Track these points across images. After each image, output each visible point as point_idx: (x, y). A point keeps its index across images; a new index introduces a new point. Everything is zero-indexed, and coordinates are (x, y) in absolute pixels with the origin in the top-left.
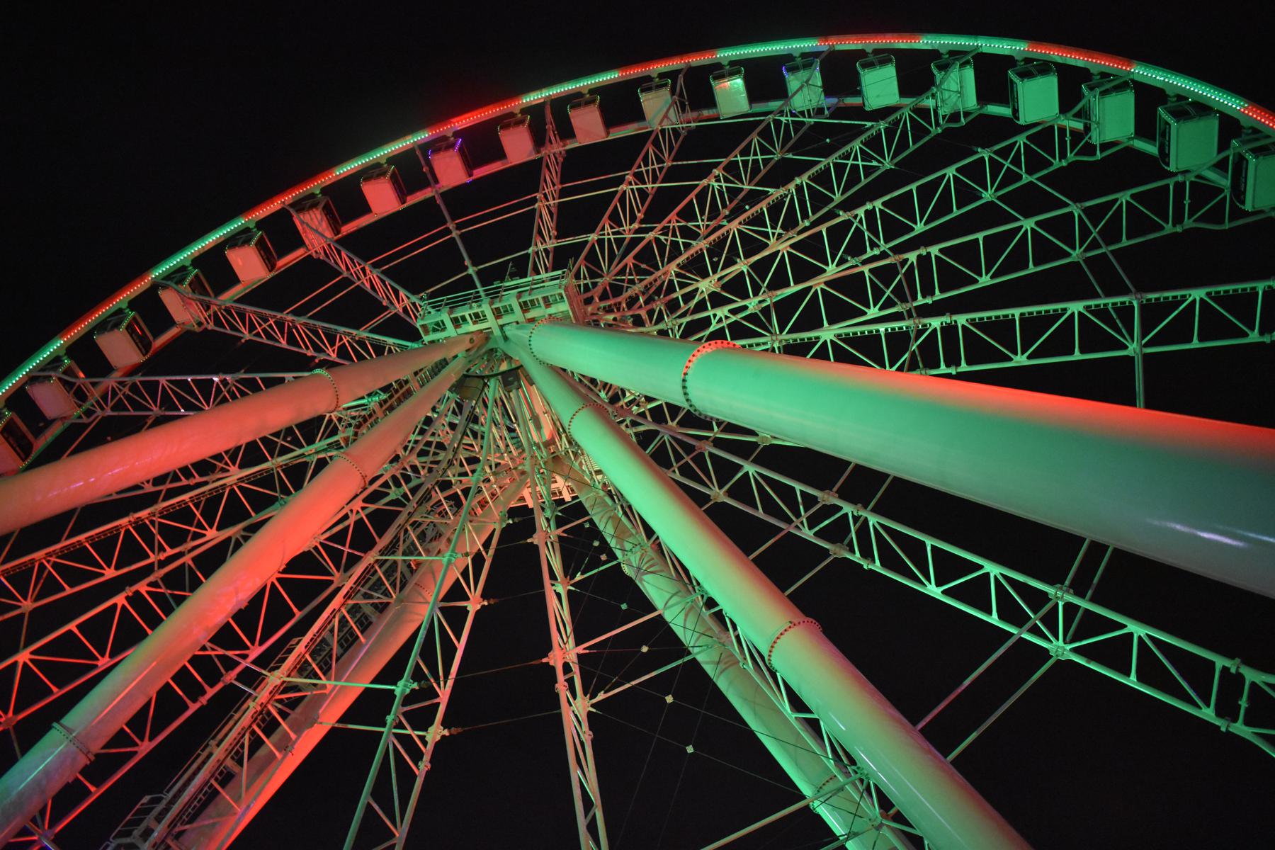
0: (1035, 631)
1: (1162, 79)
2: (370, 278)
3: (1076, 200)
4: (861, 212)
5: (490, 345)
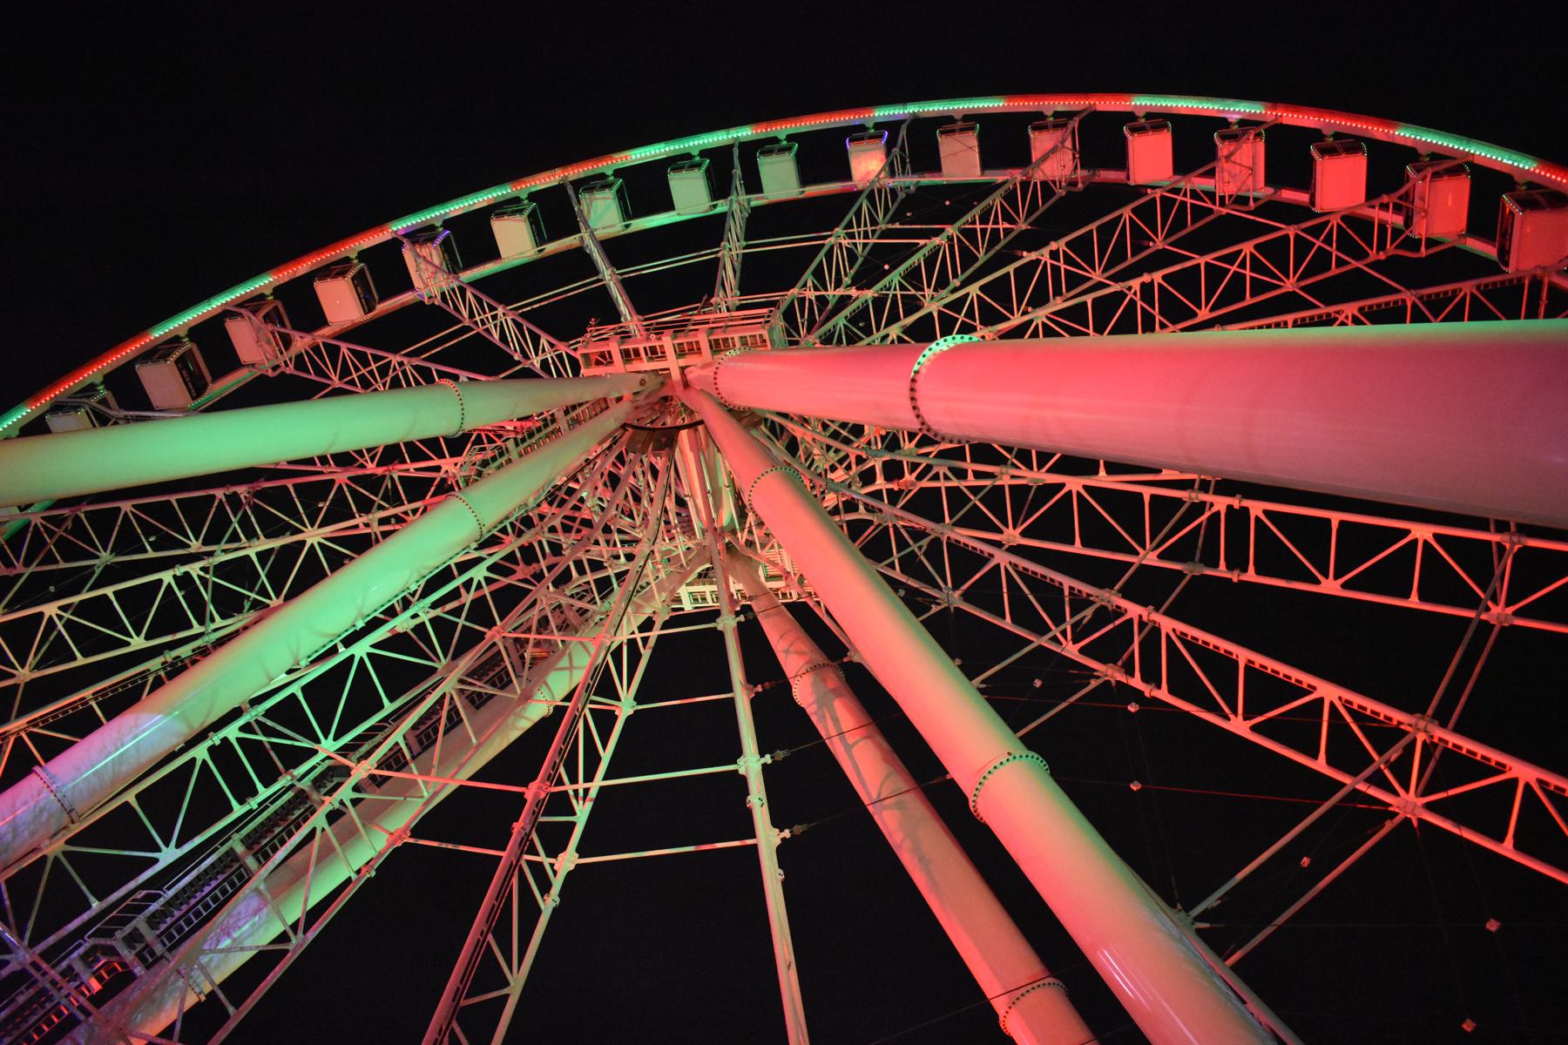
0: (1378, 780)
1: (1510, 162)
2: (501, 322)
3: (1409, 286)
4: (1135, 284)
5: (665, 392)
